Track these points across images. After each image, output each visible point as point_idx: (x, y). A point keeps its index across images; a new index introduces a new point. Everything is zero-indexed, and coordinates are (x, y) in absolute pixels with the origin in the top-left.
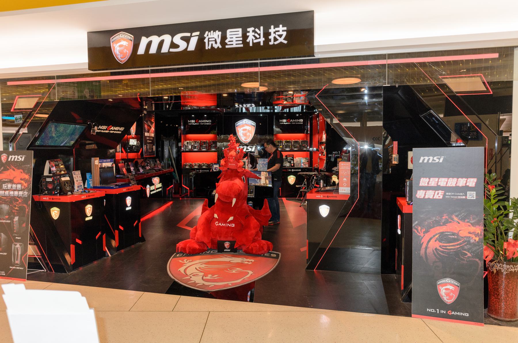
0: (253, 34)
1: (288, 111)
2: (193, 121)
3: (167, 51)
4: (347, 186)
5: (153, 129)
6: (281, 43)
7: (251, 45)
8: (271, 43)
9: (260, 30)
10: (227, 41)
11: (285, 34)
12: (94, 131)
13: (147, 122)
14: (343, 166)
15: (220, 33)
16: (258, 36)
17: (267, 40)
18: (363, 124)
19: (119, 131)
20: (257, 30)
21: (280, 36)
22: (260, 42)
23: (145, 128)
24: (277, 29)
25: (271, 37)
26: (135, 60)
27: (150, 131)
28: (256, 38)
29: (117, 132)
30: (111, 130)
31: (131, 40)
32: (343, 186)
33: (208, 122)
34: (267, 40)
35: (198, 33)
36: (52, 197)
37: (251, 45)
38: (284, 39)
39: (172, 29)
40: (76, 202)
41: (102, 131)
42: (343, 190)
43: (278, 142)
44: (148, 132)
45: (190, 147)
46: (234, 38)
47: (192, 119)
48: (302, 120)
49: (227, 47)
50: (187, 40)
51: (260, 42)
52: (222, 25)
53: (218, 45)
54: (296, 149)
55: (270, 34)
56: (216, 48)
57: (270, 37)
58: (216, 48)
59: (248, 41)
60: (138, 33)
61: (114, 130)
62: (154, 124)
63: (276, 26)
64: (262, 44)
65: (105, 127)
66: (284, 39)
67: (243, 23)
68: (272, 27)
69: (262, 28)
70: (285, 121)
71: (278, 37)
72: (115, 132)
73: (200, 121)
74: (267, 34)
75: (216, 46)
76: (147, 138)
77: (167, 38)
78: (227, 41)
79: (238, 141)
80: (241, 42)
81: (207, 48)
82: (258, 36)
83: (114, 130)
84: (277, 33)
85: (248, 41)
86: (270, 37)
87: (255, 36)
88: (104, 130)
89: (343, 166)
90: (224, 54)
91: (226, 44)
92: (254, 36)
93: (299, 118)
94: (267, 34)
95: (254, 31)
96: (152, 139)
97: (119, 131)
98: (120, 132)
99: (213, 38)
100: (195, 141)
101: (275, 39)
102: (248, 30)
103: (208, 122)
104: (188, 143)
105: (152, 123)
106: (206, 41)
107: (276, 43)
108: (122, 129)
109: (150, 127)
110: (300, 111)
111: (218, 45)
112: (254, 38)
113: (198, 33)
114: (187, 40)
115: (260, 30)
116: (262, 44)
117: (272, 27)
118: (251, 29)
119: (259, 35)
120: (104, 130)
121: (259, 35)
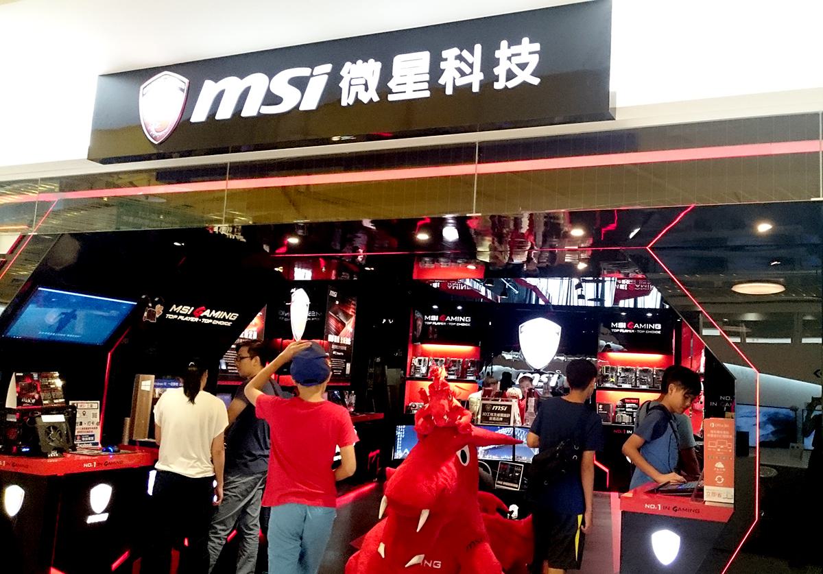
0: (458, 64)
1: (632, 306)
2: (435, 318)
3: (254, 113)
4: (725, 485)
5: (350, 327)
6: (524, 84)
7: (449, 91)
8: (498, 86)
9: (472, 53)
10: (391, 84)
11: (534, 61)
12: (151, 315)
13: (336, 313)
14: (715, 428)
15: (379, 65)
16: (467, 69)
17: (490, 79)
18: (797, 341)
19: (224, 319)
20: (465, 54)
21: (523, 66)
22: (470, 85)
23: (329, 325)
24: (515, 49)
25: (500, 71)
26: (187, 136)
27: (342, 333)
28: (463, 74)
29: (220, 323)
30: (205, 317)
31: (183, 90)
32: (714, 484)
33: (464, 321)
34: (490, 79)
35: (328, 68)
36: (16, 460)
37: (449, 91)
38: (533, 74)
39: (269, 61)
40: (67, 476)
41: (181, 318)
42: (714, 494)
43: (607, 368)
44: (337, 333)
45: (424, 370)
46: (410, 76)
47: (434, 313)
48: (659, 326)
49: (391, 98)
50: (300, 84)
51: (470, 85)
52: (382, 46)
53: (372, 95)
54: (644, 387)
55: (496, 62)
56: (365, 101)
57: (496, 71)
58: (365, 101)
59: (441, 81)
60: (198, 71)
61: (213, 318)
62: (352, 320)
63: (514, 41)
64: (476, 89)
65: (186, 309)
66: (533, 74)
67: (432, 38)
68: (504, 44)
69: (478, 48)
70: (622, 325)
71: (516, 70)
72: (215, 322)
73: (448, 318)
74: (489, 63)
75: (365, 98)
76: (334, 347)
77: (258, 82)
78: (391, 84)
79: (521, 364)
80: (426, 86)
81: (344, 103)
82: (467, 69)
83: (213, 318)
84: (516, 60)
85: (441, 81)
86: (496, 71)
87: (460, 70)
88: (185, 315)
89: (715, 428)
90: (387, 115)
91: (391, 92)
92: (459, 70)
93: (652, 321)
94: (489, 63)
95: (460, 58)
96: (345, 348)
97: (224, 319)
98: (229, 324)
99: (359, 82)
100: (437, 357)
101: (510, 75)
102: (445, 54)
103: (464, 321)
104: (420, 361)
105: (348, 316)
106: (344, 85)
107: (512, 84)
108: (233, 316)
109: (344, 325)
110: (658, 307)
111: (372, 95)
112: (458, 75)
113: (328, 68)
114: (300, 84)
115: (472, 53)
116: (476, 89)
117: (504, 44)
118: (450, 54)
119: (471, 66)
120: (185, 315)
121: (471, 66)
